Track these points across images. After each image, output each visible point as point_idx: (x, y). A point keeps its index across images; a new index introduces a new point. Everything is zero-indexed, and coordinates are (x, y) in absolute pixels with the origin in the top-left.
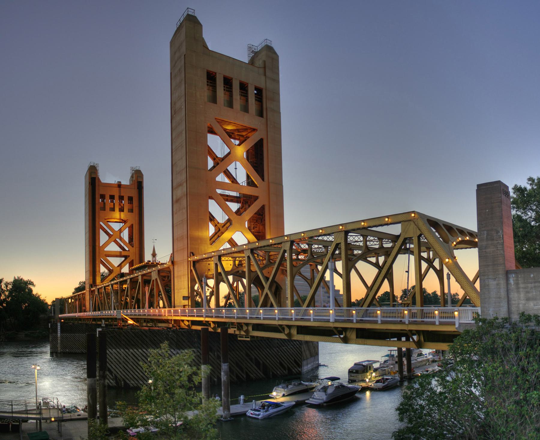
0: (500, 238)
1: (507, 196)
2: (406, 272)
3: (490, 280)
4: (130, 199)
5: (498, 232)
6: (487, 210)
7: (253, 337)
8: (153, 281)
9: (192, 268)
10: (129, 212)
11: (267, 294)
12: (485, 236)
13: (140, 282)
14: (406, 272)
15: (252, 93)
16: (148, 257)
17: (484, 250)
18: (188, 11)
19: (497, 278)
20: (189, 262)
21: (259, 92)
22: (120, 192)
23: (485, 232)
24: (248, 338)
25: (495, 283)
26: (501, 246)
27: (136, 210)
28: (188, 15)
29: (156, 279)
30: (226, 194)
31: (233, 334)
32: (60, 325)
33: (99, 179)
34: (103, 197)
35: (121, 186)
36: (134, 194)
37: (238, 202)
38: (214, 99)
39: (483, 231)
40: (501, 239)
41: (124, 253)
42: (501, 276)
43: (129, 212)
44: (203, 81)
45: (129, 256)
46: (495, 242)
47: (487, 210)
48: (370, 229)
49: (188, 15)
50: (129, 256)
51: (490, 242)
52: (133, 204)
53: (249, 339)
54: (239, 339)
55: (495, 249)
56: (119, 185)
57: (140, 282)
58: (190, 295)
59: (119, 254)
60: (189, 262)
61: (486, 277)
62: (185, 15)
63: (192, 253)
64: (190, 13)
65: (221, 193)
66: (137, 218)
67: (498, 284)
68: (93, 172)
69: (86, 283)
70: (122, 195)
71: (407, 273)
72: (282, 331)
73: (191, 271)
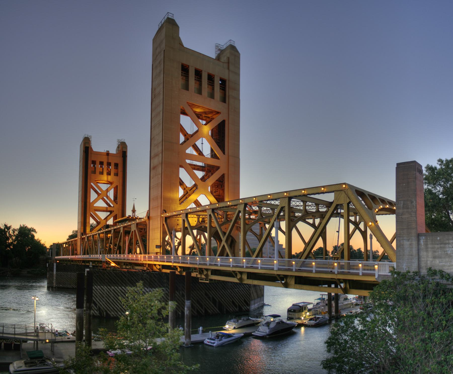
0: (414, 207)
1: (420, 173)
2: (337, 232)
3: (404, 241)
4: (116, 165)
5: (412, 202)
6: (404, 185)
7: (211, 280)
8: (133, 232)
9: (164, 223)
10: (114, 175)
11: (224, 245)
12: (402, 205)
13: (121, 233)
14: (337, 232)
15: (217, 83)
16: (129, 213)
17: (400, 217)
18: (168, 15)
19: (410, 239)
20: (162, 218)
21: (223, 82)
22: (108, 159)
23: (402, 202)
24: (208, 280)
25: (408, 243)
26: (414, 214)
27: (120, 174)
28: (168, 18)
29: (135, 231)
30: (194, 164)
31: (195, 277)
32: (55, 265)
33: (91, 148)
34: (94, 162)
35: (110, 155)
36: (119, 161)
37: (202, 170)
38: (186, 87)
39: (400, 201)
40: (415, 208)
41: (109, 209)
42: (413, 238)
43: (114, 175)
44: (178, 72)
45: (113, 211)
46: (410, 210)
47: (404, 185)
48: (309, 196)
49: (168, 18)
50: (113, 211)
51: (405, 210)
52: (118, 169)
53: (208, 282)
54: (200, 281)
55: (409, 216)
56: (108, 154)
57: (121, 233)
58: (161, 245)
59: (105, 209)
60: (162, 218)
61: (401, 238)
62: (166, 18)
63: (165, 211)
64: (170, 17)
65: (190, 163)
66: (121, 181)
67: (411, 244)
68: (87, 142)
69: (78, 232)
70: (110, 161)
71: (337, 233)
72: (235, 276)
73: (163, 225)
